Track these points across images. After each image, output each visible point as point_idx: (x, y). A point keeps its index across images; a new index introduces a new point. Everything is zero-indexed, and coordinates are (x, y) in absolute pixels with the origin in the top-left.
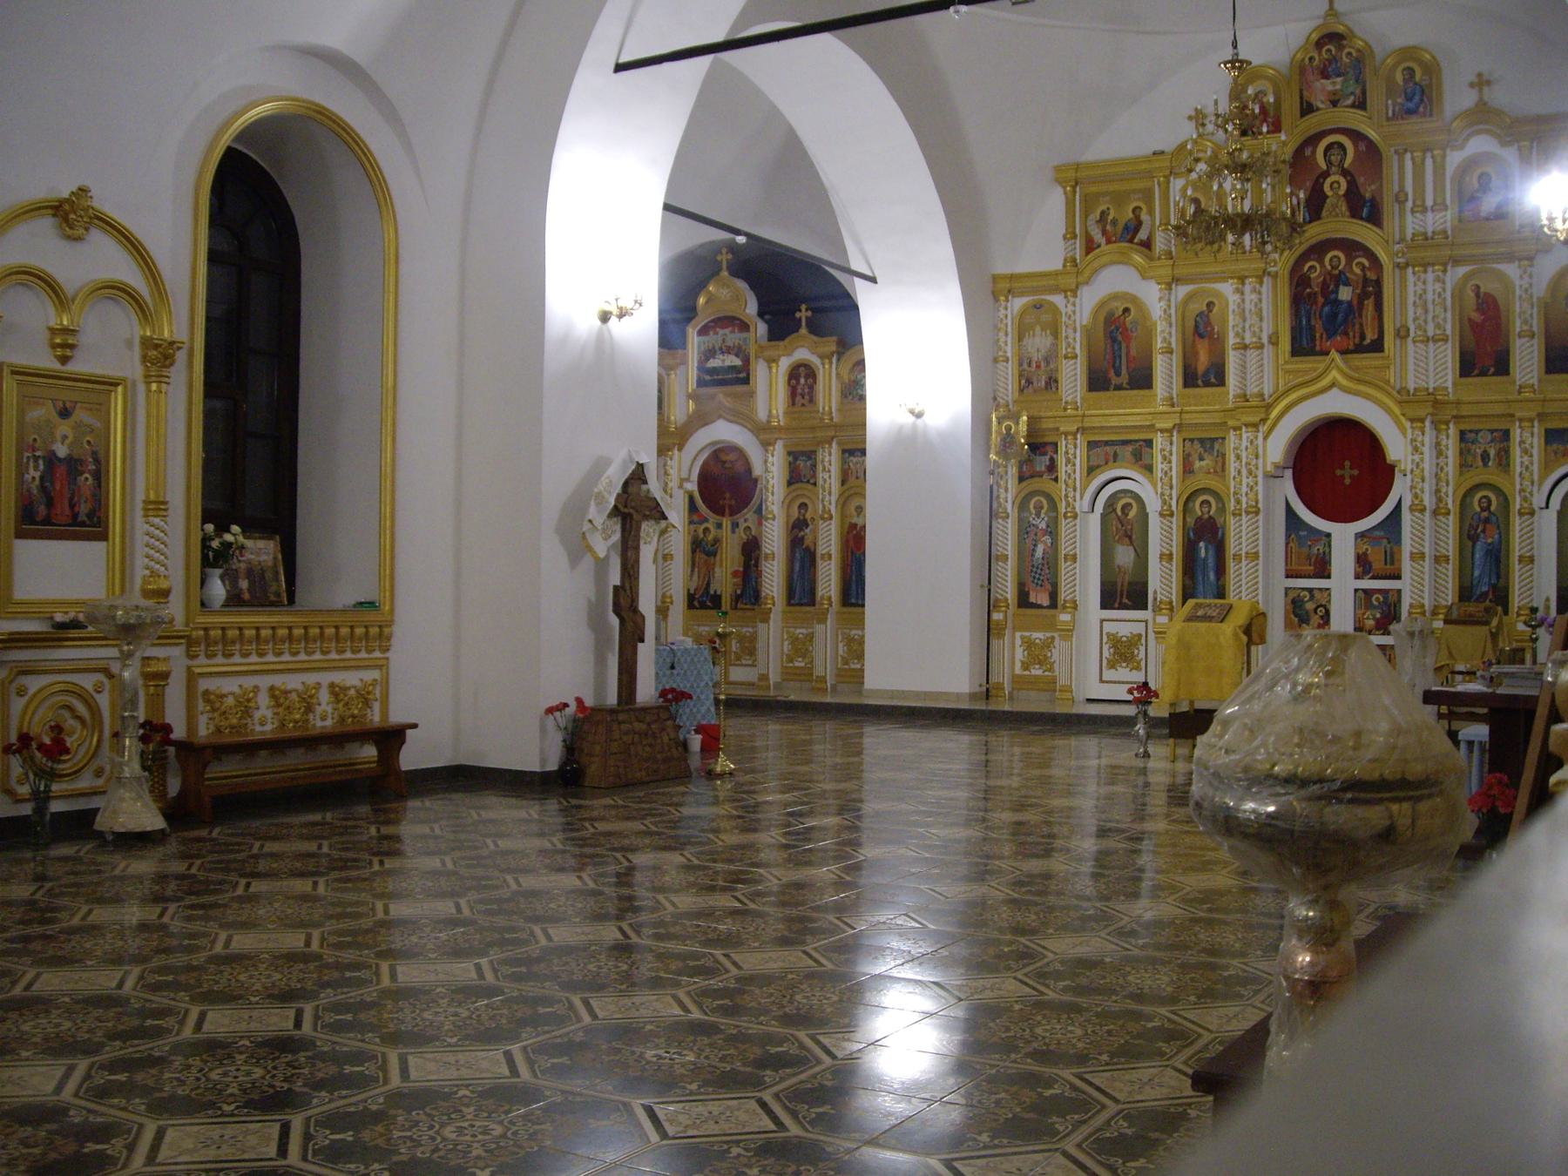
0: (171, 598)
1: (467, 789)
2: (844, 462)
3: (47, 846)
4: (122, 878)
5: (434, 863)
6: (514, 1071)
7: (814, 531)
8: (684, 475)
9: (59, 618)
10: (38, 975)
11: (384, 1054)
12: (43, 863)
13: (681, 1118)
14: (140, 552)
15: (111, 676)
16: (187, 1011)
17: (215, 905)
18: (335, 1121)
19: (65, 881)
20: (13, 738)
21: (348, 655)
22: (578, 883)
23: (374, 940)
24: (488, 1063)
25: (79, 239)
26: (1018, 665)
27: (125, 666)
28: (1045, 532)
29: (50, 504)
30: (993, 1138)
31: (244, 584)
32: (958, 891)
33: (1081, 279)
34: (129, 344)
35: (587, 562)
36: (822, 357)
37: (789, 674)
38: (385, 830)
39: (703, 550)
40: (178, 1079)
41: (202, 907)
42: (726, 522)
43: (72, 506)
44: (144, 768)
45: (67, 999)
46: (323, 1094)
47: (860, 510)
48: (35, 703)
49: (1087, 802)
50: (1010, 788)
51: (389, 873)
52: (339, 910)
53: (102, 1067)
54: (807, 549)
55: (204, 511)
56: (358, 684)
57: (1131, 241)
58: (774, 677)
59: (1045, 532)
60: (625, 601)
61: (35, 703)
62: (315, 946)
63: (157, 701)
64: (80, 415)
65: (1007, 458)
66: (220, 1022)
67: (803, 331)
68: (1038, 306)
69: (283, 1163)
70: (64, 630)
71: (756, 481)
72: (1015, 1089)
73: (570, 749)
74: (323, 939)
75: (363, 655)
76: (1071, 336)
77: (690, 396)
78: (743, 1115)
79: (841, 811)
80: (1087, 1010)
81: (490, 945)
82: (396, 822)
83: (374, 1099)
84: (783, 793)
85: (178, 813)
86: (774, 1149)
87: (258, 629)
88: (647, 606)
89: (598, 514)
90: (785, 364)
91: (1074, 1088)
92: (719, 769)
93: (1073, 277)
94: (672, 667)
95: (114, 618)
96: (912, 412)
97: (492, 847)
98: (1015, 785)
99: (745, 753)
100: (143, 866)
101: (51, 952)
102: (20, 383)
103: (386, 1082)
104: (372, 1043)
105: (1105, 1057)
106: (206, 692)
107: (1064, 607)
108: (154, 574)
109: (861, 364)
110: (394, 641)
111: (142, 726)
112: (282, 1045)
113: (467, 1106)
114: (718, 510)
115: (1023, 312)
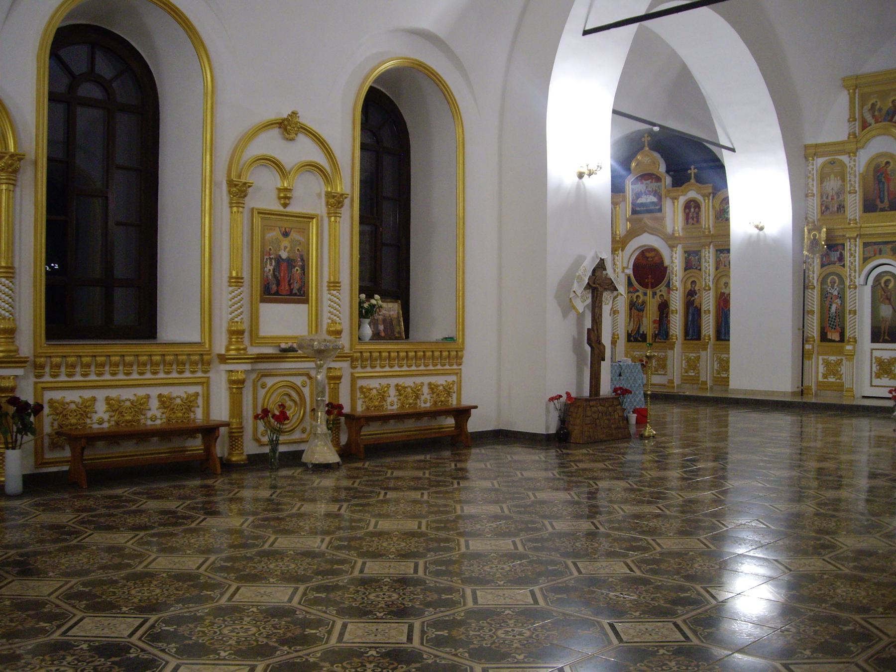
1: (505, 443)
2: (717, 257)
3: (277, 470)
4: (317, 488)
5: (487, 484)
6: (536, 601)
7: (700, 297)
8: (625, 265)
9: (283, 346)
10: (276, 539)
11: (463, 589)
12: (275, 479)
13: (631, 631)
14: (326, 309)
15: (310, 378)
16: (356, 562)
17: (368, 505)
18: (437, 624)
19: (287, 489)
20: (259, 412)
21: (439, 367)
22: (569, 497)
23: (450, 526)
24: (521, 596)
25: (292, 140)
26: (820, 375)
27: (318, 373)
28: (838, 297)
29: (278, 284)
30: (813, 653)
31: (381, 327)
32: (784, 507)
33: (859, 145)
34: (319, 195)
35: (572, 316)
36: (703, 196)
37: (686, 380)
38: (459, 465)
39: (636, 308)
41: (361, 505)
42: (649, 292)
43: (290, 285)
44: (329, 429)
46: (431, 609)
47: (727, 284)
48: (271, 391)
49: (863, 457)
50: (816, 448)
51: (459, 489)
52: (436, 509)
53: (312, 589)
54: (696, 307)
55: (360, 287)
56: (444, 383)
57: (891, 121)
58: (677, 381)
59: (838, 297)
60: (594, 337)
61: (271, 391)
62: (424, 528)
63: (335, 392)
64: (294, 235)
65: (814, 253)
66: (373, 568)
67: (693, 181)
68: (832, 163)
70: (286, 353)
71: (666, 268)
72: (826, 624)
73: (563, 421)
74: (427, 525)
75: (447, 367)
76: (853, 179)
77: (627, 220)
78: (662, 631)
79: (716, 459)
80: (868, 580)
82: (466, 461)
83: (459, 613)
84: (683, 448)
85: (346, 453)
86: (683, 652)
87: (389, 352)
88: (606, 340)
89: (578, 288)
90: (682, 200)
91: (862, 627)
92: (647, 434)
93: (854, 143)
94: (620, 375)
95: (313, 346)
96: (757, 227)
97: (520, 476)
98: (819, 446)
99: (660, 425)
100: (328, 482)
101: (282, 527)
102: (262, 218)
104: (457, 583)
105: (880, 610)
106: (361, 388)
107: (849, 341)
108: (333, 322)
109: (726, 200)
110: (464, 359)
111: (327, 405)
112: (403, 582)
113: (510, 619)
114: (645, 286)
115: (823, 167)
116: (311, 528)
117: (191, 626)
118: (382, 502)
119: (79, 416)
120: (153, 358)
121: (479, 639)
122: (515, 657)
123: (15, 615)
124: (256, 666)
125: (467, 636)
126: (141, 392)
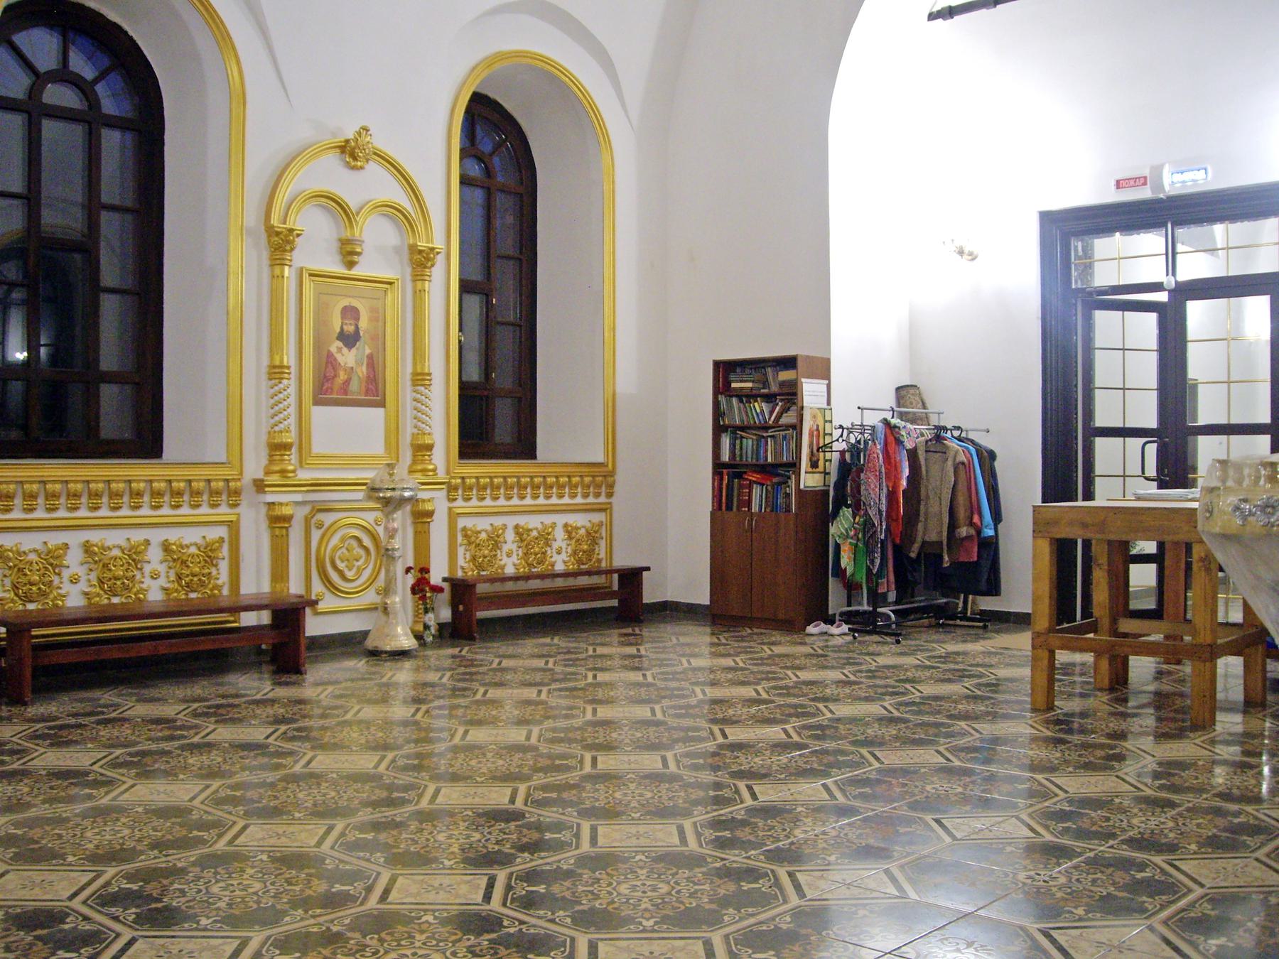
30: (1087, 912)
40: (413, 840)
45: (334, 776)
48: (329, 534)
69: (488, 907)
81: (676, 741)
83: (566, 860)
97: (686, 665)
100: (403, 674)
104: (571, 816)
119: (43, 571)
120: (114, 485)
121: (590, 896)
122: (640, 923)
123: (12, 939)
124: (250, 938)
125: (573, 893)
126: (138, 536)
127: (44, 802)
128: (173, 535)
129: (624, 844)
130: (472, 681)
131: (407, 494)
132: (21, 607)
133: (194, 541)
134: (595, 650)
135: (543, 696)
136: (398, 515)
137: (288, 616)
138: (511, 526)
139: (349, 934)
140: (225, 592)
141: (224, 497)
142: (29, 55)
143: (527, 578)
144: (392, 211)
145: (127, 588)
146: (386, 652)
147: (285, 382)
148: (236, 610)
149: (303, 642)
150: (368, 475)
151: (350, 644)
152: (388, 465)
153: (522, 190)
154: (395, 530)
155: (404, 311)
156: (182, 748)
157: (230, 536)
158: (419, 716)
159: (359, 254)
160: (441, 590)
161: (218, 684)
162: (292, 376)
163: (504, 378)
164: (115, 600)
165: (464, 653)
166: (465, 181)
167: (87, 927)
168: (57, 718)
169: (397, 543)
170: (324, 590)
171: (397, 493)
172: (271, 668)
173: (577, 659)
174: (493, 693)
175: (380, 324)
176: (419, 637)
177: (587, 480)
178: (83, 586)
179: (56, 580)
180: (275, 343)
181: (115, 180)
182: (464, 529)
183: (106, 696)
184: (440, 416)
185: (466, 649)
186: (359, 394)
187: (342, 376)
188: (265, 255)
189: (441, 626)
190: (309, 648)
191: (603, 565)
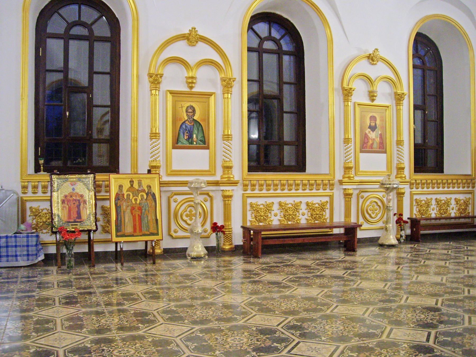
0: (233, 169)
16: (403, 296)
69: (427, 344)
74: (447, 280)
100: (392, 253)
103: (463, 324)
108: (225, 161)
116: (380, 278)
117: (309, 323)
118: (422, 266)
121: (469, 344)
124: (340, 346)
125: (463, 342)
126: (297, 200)
127: (267, 292)
128: (310, 200)
129: (401, 338)
130: (419, 257)
131: (395, 186)
132: (257, 224)
133: (290, 202)
134: (467, 248)
135: (447, 265)
136: (391, 194)
137: (351, 231)
138: (283, 202)
139: (376, 348)
140: (328, 221)
141: (328, 186)
142: (258, 32)
143: (440, 219)
144: (388, 80)
145: (293, 218)
146: (386, 245)
147: (350, 144)
148: (331, 227)
149: (356, 240)
150: (380, 179)
151: (373, 241)
152: (388, 175)
153: (436, 69)
154: (390, 200)
155: (393, 117)
156: (314, 276)
157: (330, 201)
158: (399, 270)
159: (376, 96)
160: (407, 222)
161: (326, 254)
162: (352, 142)
163: (431, 141)
164: (289, 223)
165: (415, 247)
166: (415, 67)
167: (283, 336)
168: (269, 263)
169: (391, 204)
170: (364, 221)
171: (391, 186)
172: (344, 249)
173: (460, 251)
174: (427, 262)
175: (384, 123)
176: (398, 240)
177: (464, 181)
178: (278, 217)
179: (269, 215)
180: (346, 130)
181: (288, 75)
182: (416, 199)
183: (286, 256)
184: (407, 157)
185: (416, 245)
186: (377, 148)
187: (371, 142)
188: (342, 98)
189: (407, 236)
190: (358, 242)
191: (470, 214)
